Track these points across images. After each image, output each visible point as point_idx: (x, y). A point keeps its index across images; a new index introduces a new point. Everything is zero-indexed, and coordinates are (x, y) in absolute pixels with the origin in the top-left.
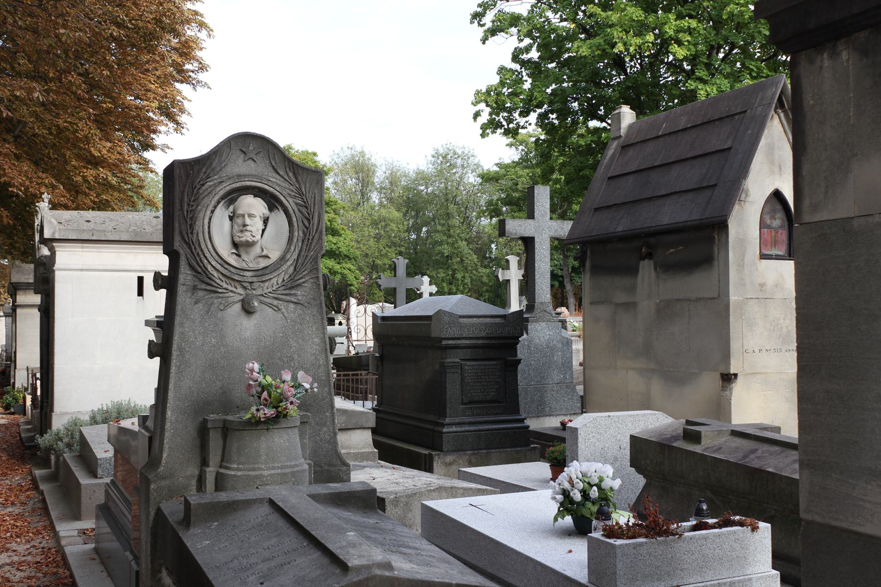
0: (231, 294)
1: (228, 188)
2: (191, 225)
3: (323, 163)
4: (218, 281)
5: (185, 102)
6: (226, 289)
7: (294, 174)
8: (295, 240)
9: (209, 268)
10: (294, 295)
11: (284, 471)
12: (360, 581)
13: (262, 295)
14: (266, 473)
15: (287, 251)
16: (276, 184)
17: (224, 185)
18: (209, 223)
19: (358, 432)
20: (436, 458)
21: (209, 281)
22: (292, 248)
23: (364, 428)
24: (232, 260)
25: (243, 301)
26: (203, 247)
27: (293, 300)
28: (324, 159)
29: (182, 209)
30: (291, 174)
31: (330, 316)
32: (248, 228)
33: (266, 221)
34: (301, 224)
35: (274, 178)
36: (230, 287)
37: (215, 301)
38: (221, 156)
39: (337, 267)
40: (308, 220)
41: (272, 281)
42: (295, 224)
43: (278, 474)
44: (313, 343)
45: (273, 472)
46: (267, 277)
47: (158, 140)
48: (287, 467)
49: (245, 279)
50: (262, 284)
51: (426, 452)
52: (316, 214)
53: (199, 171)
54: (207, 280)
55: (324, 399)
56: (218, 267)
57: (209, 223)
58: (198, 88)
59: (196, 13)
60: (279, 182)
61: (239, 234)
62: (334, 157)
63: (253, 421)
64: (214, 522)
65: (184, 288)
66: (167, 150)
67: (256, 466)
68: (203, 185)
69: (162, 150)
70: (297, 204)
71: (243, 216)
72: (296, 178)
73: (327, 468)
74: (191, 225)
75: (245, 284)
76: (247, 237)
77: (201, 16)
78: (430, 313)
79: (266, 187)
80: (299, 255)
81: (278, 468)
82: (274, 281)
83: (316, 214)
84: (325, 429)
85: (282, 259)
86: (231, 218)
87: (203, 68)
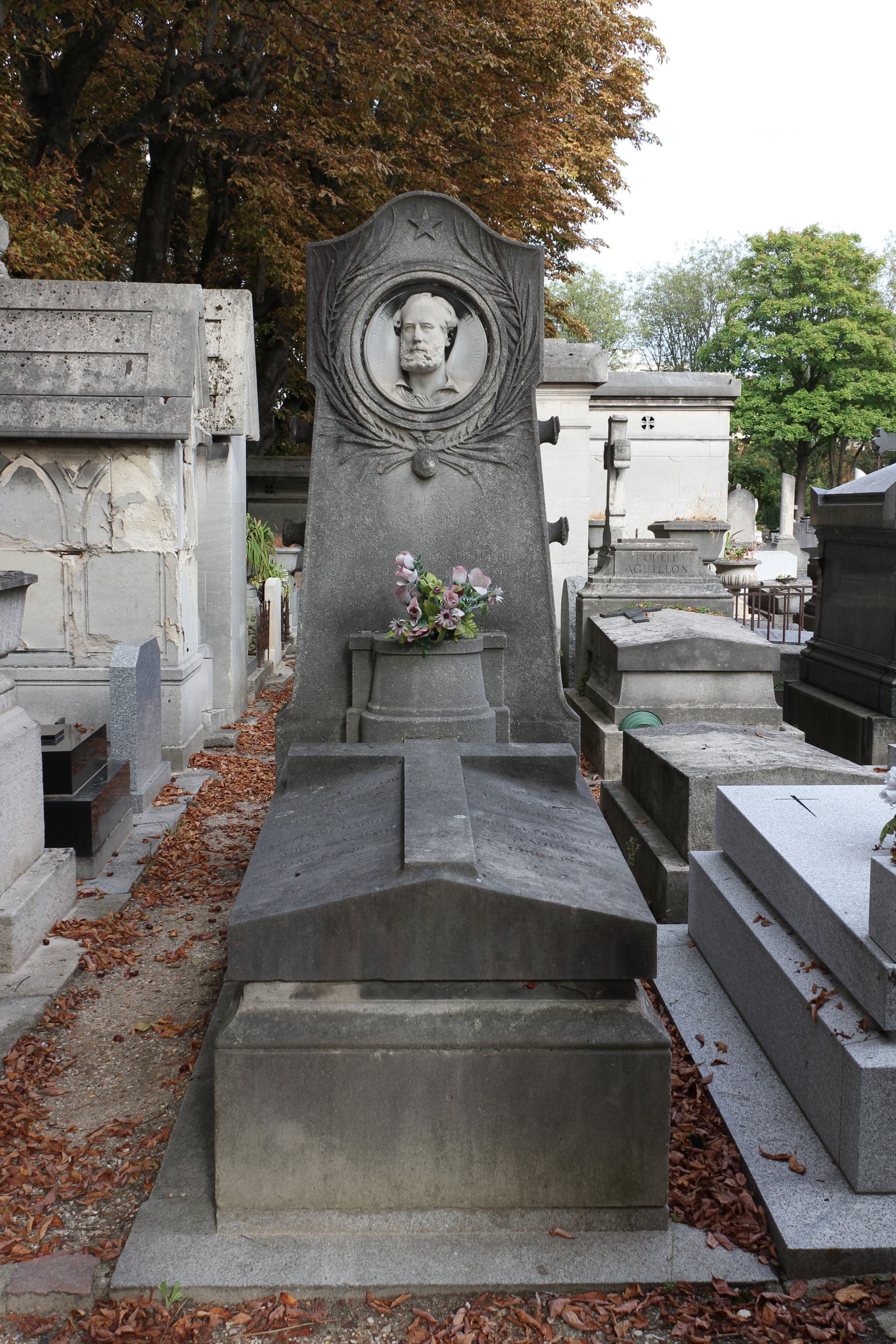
1: (389, 284)
2: (332, 344)
5: (618, 167)
7: (496, 256)
8: (495, 363)
9: (361, 409)
10: (494, 450)
11: (445, 720)
12: (414, 887)
13: (443, 451)
14: (418, 720)
15: (483, 380)
16: (463, 271)
17: (384, 278)
18: (362, 340)
19: (751, 677)
20: (878, 726)
21: (360, 429)
22: (491, 377)
24: (398, 397)
25: (412, 459)
26: (352, 377)
27: (492, 457)
28: (872, 245)
29: (318, 320)
30: (490, 256)
33: (452, 334)
34: (505, 337)
35: (463, 264)
36: (393, 439)
37: (371, 460)
38: (378, 233)
40: (518, 329)
41: (459, 429)
42: (496, 336)
44: (522, 526)
46: (450, 423)
47: (588, 230)
48: (452, 714)
49: (415, 426)
50: (443, 434)
51: (863, 714)
53: (346, 257)
54: (360, 429)
55: (539, 615)
56: (375, 407)
57: (362, 340)
58: (644, 144)
63: (402, 642)
64: (320, 785)
65: (323, 441)
66: (601, 248)
67: (405, 709)
68: (352, 280)
69: (594, 247)
70: (499, 304)
71: (414, 326)
72: (499, 262)
73: (541, 720)
74: (332, 344)
76: (419, 360)
78: (884, 490)
79: (450, 279)
80: (501, 387)
81: (438, 714)
82: (462, 428)
84: (539, 661)
85: (476, 394)
86: (398, 331)
87: (648, 111)
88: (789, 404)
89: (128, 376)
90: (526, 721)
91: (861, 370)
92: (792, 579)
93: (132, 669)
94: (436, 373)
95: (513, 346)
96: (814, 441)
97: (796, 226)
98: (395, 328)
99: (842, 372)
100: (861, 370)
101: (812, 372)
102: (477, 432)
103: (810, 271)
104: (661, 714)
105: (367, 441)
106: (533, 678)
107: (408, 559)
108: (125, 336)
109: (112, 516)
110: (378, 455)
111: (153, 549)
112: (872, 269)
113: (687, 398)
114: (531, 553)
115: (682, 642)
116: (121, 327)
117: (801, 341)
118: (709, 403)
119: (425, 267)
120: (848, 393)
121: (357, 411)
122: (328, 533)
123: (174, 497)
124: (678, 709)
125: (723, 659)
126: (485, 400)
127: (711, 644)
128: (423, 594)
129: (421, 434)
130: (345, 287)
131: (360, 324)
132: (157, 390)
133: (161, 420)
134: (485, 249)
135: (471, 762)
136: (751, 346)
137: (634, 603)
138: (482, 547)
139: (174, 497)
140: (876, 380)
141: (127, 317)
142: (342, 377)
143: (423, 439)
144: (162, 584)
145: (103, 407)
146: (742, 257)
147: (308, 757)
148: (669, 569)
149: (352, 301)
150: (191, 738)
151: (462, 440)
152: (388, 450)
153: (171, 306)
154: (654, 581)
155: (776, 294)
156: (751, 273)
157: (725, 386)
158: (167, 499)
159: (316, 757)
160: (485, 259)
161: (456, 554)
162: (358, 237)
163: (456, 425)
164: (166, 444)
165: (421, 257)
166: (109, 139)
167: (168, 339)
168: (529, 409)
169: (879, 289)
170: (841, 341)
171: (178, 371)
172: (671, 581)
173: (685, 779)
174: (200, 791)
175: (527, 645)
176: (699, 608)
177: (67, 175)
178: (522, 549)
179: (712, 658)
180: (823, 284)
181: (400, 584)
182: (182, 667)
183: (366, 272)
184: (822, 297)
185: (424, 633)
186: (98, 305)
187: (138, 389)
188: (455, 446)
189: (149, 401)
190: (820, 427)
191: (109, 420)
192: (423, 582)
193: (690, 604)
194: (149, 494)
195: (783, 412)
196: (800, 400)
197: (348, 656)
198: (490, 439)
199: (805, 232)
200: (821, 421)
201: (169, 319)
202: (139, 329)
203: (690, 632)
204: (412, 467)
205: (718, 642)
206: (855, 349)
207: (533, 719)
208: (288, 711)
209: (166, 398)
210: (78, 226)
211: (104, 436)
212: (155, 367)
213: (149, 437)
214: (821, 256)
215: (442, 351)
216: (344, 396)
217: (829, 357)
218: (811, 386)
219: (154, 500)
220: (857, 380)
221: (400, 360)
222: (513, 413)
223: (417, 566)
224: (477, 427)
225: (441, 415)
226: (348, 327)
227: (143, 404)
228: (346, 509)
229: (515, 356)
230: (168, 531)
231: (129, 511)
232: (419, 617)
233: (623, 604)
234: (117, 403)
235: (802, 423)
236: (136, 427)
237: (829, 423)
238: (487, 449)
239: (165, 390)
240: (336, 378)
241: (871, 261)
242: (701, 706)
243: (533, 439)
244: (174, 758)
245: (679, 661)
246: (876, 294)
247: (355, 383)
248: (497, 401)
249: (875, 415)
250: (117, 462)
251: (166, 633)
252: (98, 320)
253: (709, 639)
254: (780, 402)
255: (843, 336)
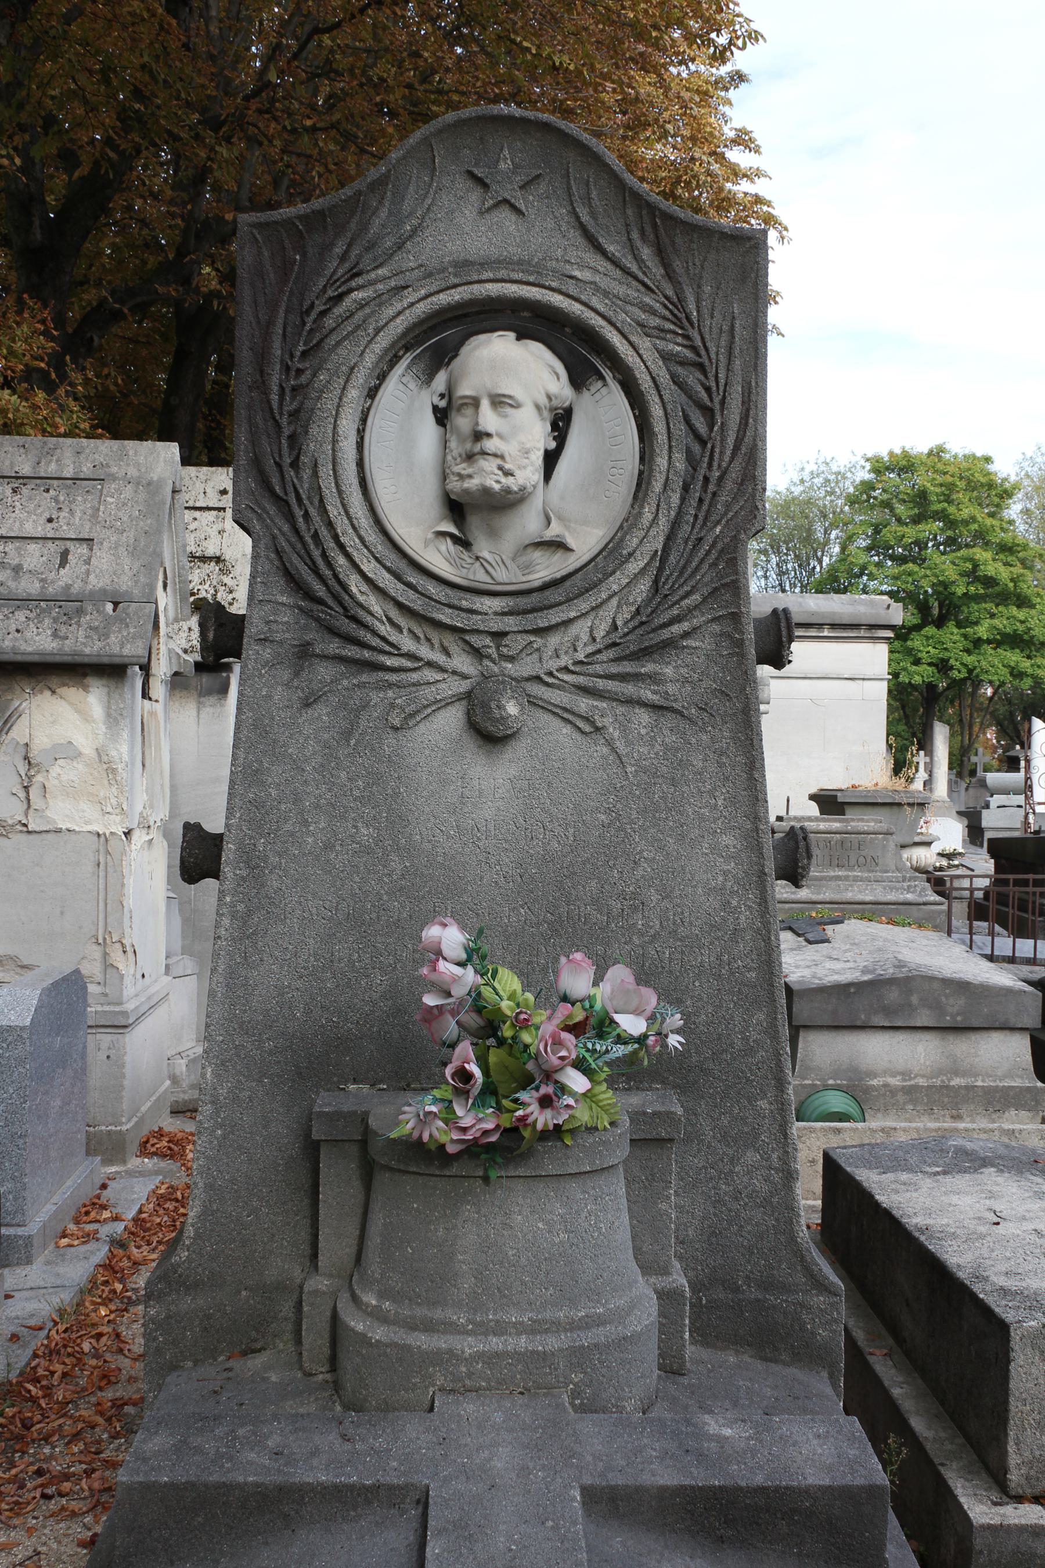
0: (430, 675)
1: (422, 308)
3: (1004, 475)
4: (384, 629)
6: (411, 656)
7: (660, 252)
8: (657, 486)
9: (355, 584)
10: (653, 678)
13: (538, 679)
14: (469, 1345)
15: (627, 525)
16: (591, 286)
18: (361, 433)
19: (996, 1037)
21: (351, 628)
22: (648, 515)
23: (1013, 1029)
24: (439, 558)
25: (468, 696)
26: (334, 511)
27: (648, 694)
29: (261, 385)
30: (646, 252)
31: (1011, 753)
32: (490, 445)
33: (561, 422)
34: (680, 428)
35: (588, 268)
36: (425, 652)
37: (375, 697)
39: (1026, 665)
40: (708, 412)
41: (574, 630)
42: (659, 427)
43: (518, 1356)
45: (496, 1343)
46: (555, 617)
48: (556, 1327)
50: (538, 642)
52: (736, 391)
53: (326, 248)
54: (351, 628)
55: (750, 1051)
56: (385, 579)
57: (361, 433)
59: (758, 200)
60: (603, 282)
61: (462, 468)
62: (1025, 464)
65: (267, 653)
67: (438, 1314)
68: (340, 298)
70: (666, 357)
71: (476, 402)
72: (666, 265)
73: (754, 1293)
74: (292, 438)
75: (476, 640)
76: (487, 476)
77: (769, 204)
79: (557, 300)
80: (670, 538)
81: (520, 1329)
82: (581, 629)
83: (736, 391)
84: (751, 1157)
85: (612, 553)
86: (442, 416)
88: (916, 642)
89: (62, 572)
90: (720, 1294)
91: (997, 606)
92: (960, 854)
93: (23, 1028)
94: (524, 508)
95: (696, 448)
96: (942, 685)
97: (921, 446)
98: (435, 409)
99: (976, 607)
100: (997, 606)
101: (941, 607)
102: (615, 637)
103: (937, 494)
104: (861, 1094)
105: (367, 654)
106: (737, 1195)
107: (451, 938)
108: (62, 514)
109: (30, 778)
110: (391, 685)
111: (89, 828)
112: (1007, 494)
113: (833, 626)
114: (735, 910)
115: (892, 981)
116: (57, 501)
117: (928, 572)
118: (862, 633)
119: (503, 274)
120: (982, 631)
121: (345, 588)
122: (274, 860)
123: (122, 750)
124: (886, 1085)
125: (955, 1007)
126: (633, 567)
127: (936, 985)
128: (488, 1026)
129: (488, 641)
130: (323, 313)
131: (354, 393)
132: (104, 591)
133: (107, 636)
134: (635, 235)
135: (608, 1503)
136: (872, 577)
137: (802, 911)
138: (622, 896)
139: (122, 750)
140: (1014, 617)
141: (68, 487)
142: (313, 512)
143: (492, 651)
144: (102, 881)
145: (21, 616)
146: (858, 480)
147: (172, 1486)
148: (853, 861)
149: (338, 343)
150: (144, 1109)
151: (580, 656)
152: (415, 676)
153: (132, 472)
154: (831, 878)
155: (899, 520)
156: (869, 497)
157: (883, 612)
158: (114, 753)
159: (191, 1485)
160: (637, 258)
161: (563, 910)
162: (354, 204)
163: (567, 623)
164: (112, 671)
165: (494, 252)
166: (115, 302)
167: (125, 519)
168: (733, 587)
169: (1014, 516)
170: (973, 574)
171: (136, 565)
172: (856, 879)
173: (1000, 1329)
174: (140, 1211)
175: (725, 1120)
176: (898, 919)
177: (38, 326)
178: (714, 902)
179: (938, 1008)
180: (952, 509)
181: (430, 1000)
182: (129, 1006)
183: (372, 283)
184: (951, 523)
185: (486, 1133)
186: (26, 470)
187: (76, 588)
188: (566, 669)
189: (90, 608)
190: (952, 668)
191: (28, 635)
192: (487, 992)
193: (883, 913)
194: (85, 744)
195: (909, 652)
196: (928, 638)
197: (312, 1150)
198: (644, 653)
199: (930, 453)
200: (952, 662)
201: (128, 492)
202: (82, 503)
203: (900, 965)
204: (469, 715)
205: (947, 982)
206: (989, 582)
207: (737, 1290)
208: (175, 1268)
209: (116, 604)
210: (50, 388)
211: (19, 658)
212: (102, 559)
213: (86, 660)
214: (949, 479)
215: (537, 458)
216: (316, 553)
217: (960, 590)
218: (940, 623)
219: (94, 754)
220: (992, 616)
221: (444, 477)
222: (696, 597)
223: (473, 956)
224: (615, 627)
225: (534, 599)
226: (328, 403)
227: (80, 612)
228: (317, 806)
229: (702, 471)
230: (114, 801)
231: (55, 770)
232: (475, 1091)
233: (787, 911)
234: (43, 611)
235: (930, 664)
236: (68, 645)
237: (962, 664)
238: (636, 677)
239: (116, 592)
240: (299, 513)
241: (1007, 485)
242: (922, 1082)
243: (742, 655)
244: (106, 1146)
245: (888, 1011)
246: (1011, 522)
247: (342, 524)
248: (660, 569)
249: (1014, 657)
250: (39, 697)
251: (105, 955)
252: (25, 491)
253: (932, 979)
254: (905, 640)
255: (976, 566)
